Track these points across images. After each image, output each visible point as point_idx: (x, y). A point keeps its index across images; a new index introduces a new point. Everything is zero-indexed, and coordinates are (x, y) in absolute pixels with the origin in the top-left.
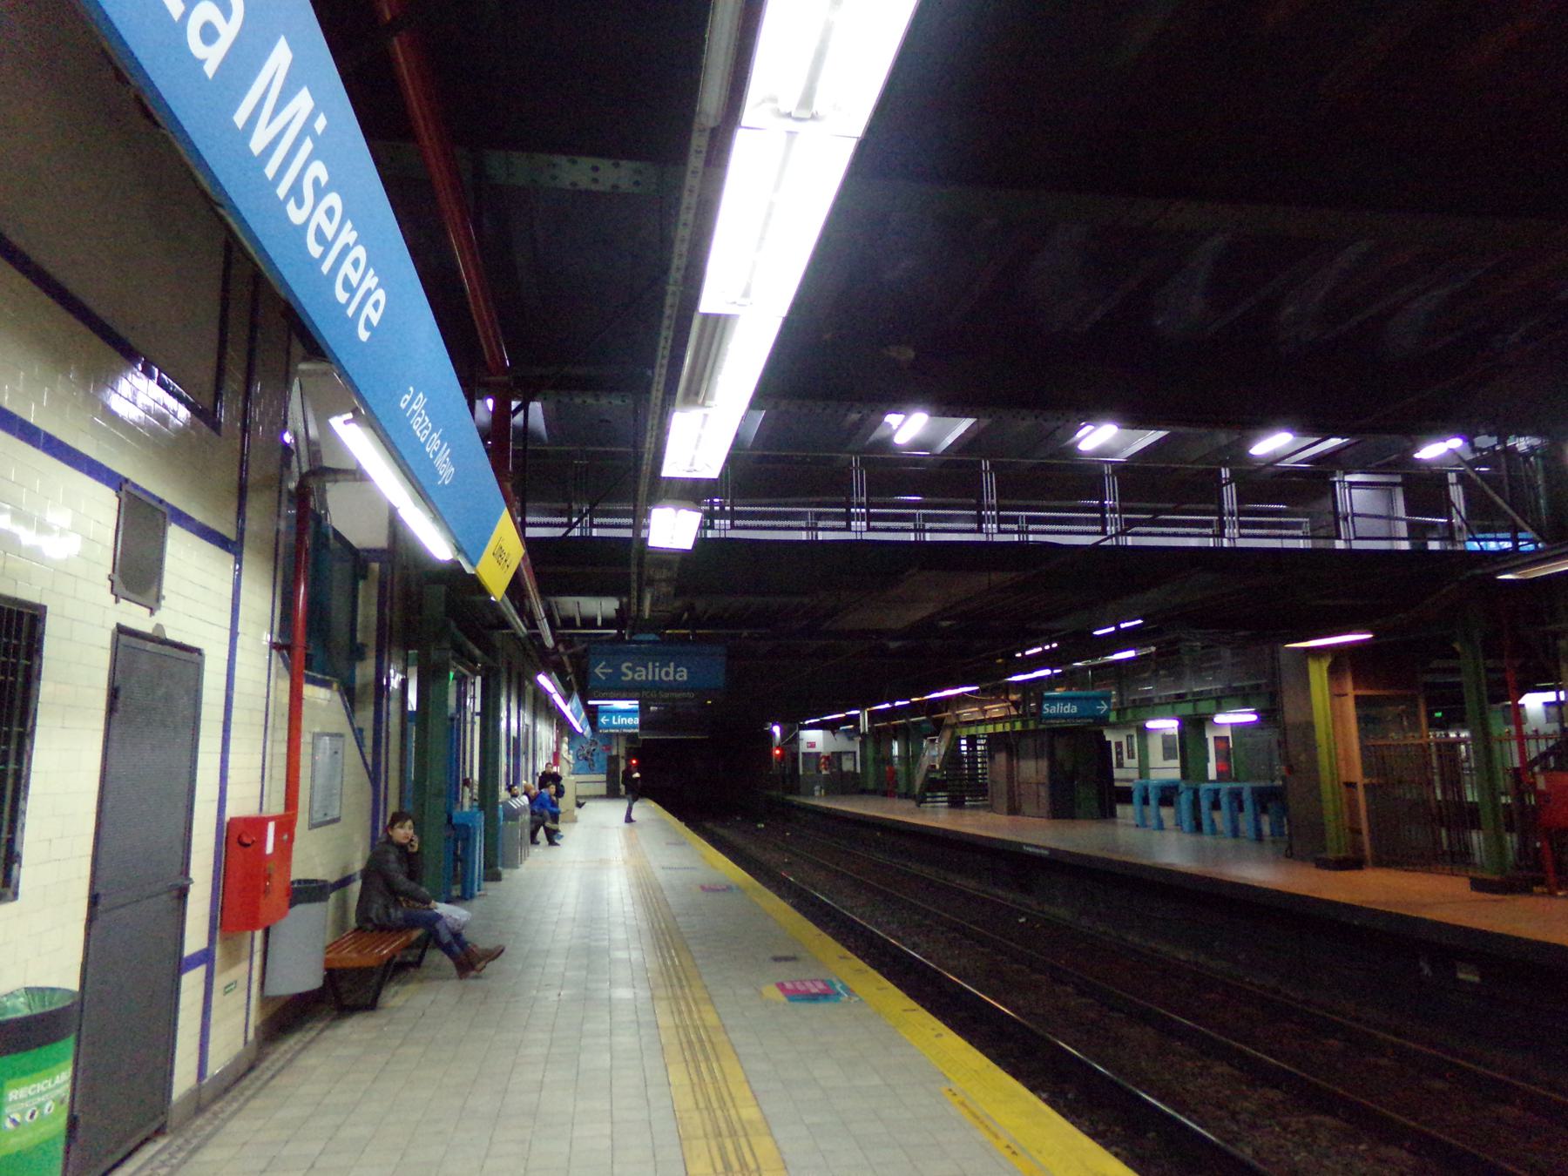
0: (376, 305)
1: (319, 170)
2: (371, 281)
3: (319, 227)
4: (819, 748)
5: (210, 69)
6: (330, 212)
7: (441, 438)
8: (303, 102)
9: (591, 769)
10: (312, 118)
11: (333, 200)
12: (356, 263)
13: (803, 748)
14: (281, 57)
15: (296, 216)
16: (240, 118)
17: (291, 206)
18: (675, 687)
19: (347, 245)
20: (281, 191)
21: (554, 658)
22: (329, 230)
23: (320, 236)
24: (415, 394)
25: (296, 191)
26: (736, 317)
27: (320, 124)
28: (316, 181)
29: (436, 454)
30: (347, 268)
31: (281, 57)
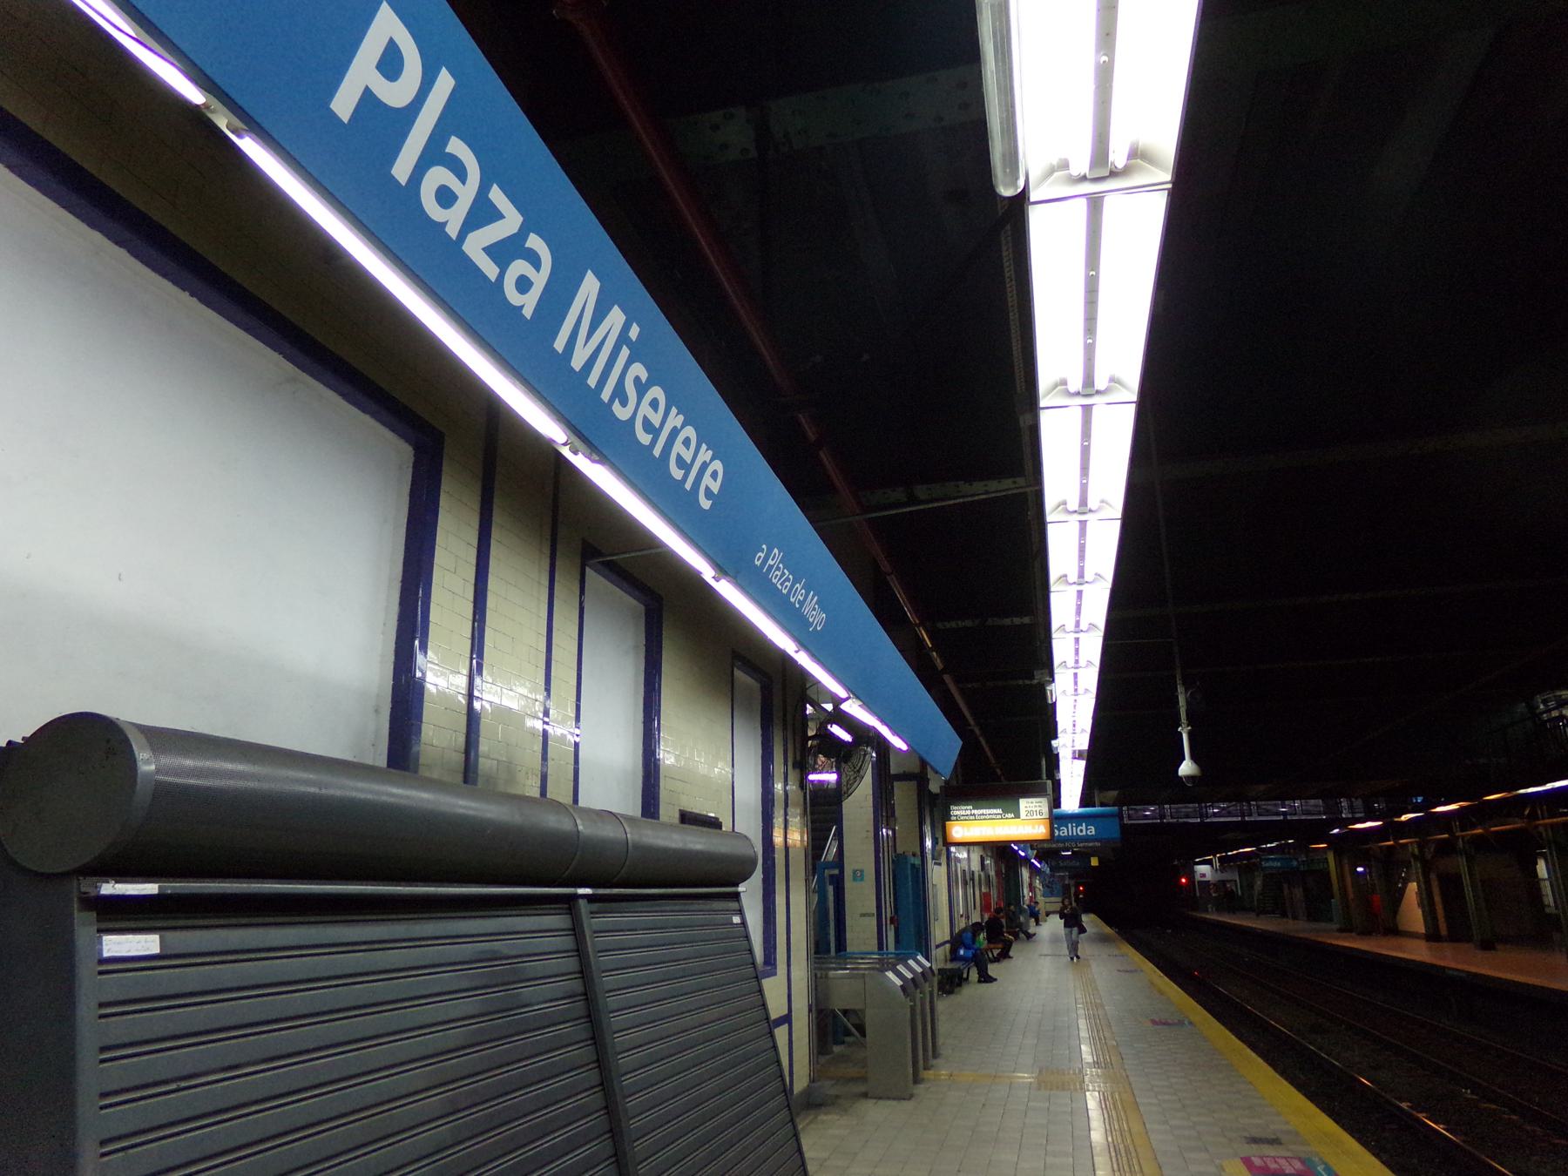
0: (714, 475)
1: (638, 370)
2: (705, 455)
3: (645, 418)
4: (1209, 877)
5: (528, 312)
6: (654, 404)
7: (807, 588)
8: (616, 317)
9: (1052, 895)
10: (626, 328)
11: (656, 392)
12: (687, 442)
13: (1198, 878)
14: (590, 286)
15: (622, 413)
16: (559, 345)
17: (616, 407)
18: (1087, 839)
19: (675, 428)
20: (606, 395)
21: (974, 975)
22: (656, 420)
23: (680, 462)
24: (770, 550)
25: (620, 394)
26: (1017, 816)
27: (634, 332)
28: (637, 379)
29: (802, 603)
30: (678, 447)
31: (590, 286)
